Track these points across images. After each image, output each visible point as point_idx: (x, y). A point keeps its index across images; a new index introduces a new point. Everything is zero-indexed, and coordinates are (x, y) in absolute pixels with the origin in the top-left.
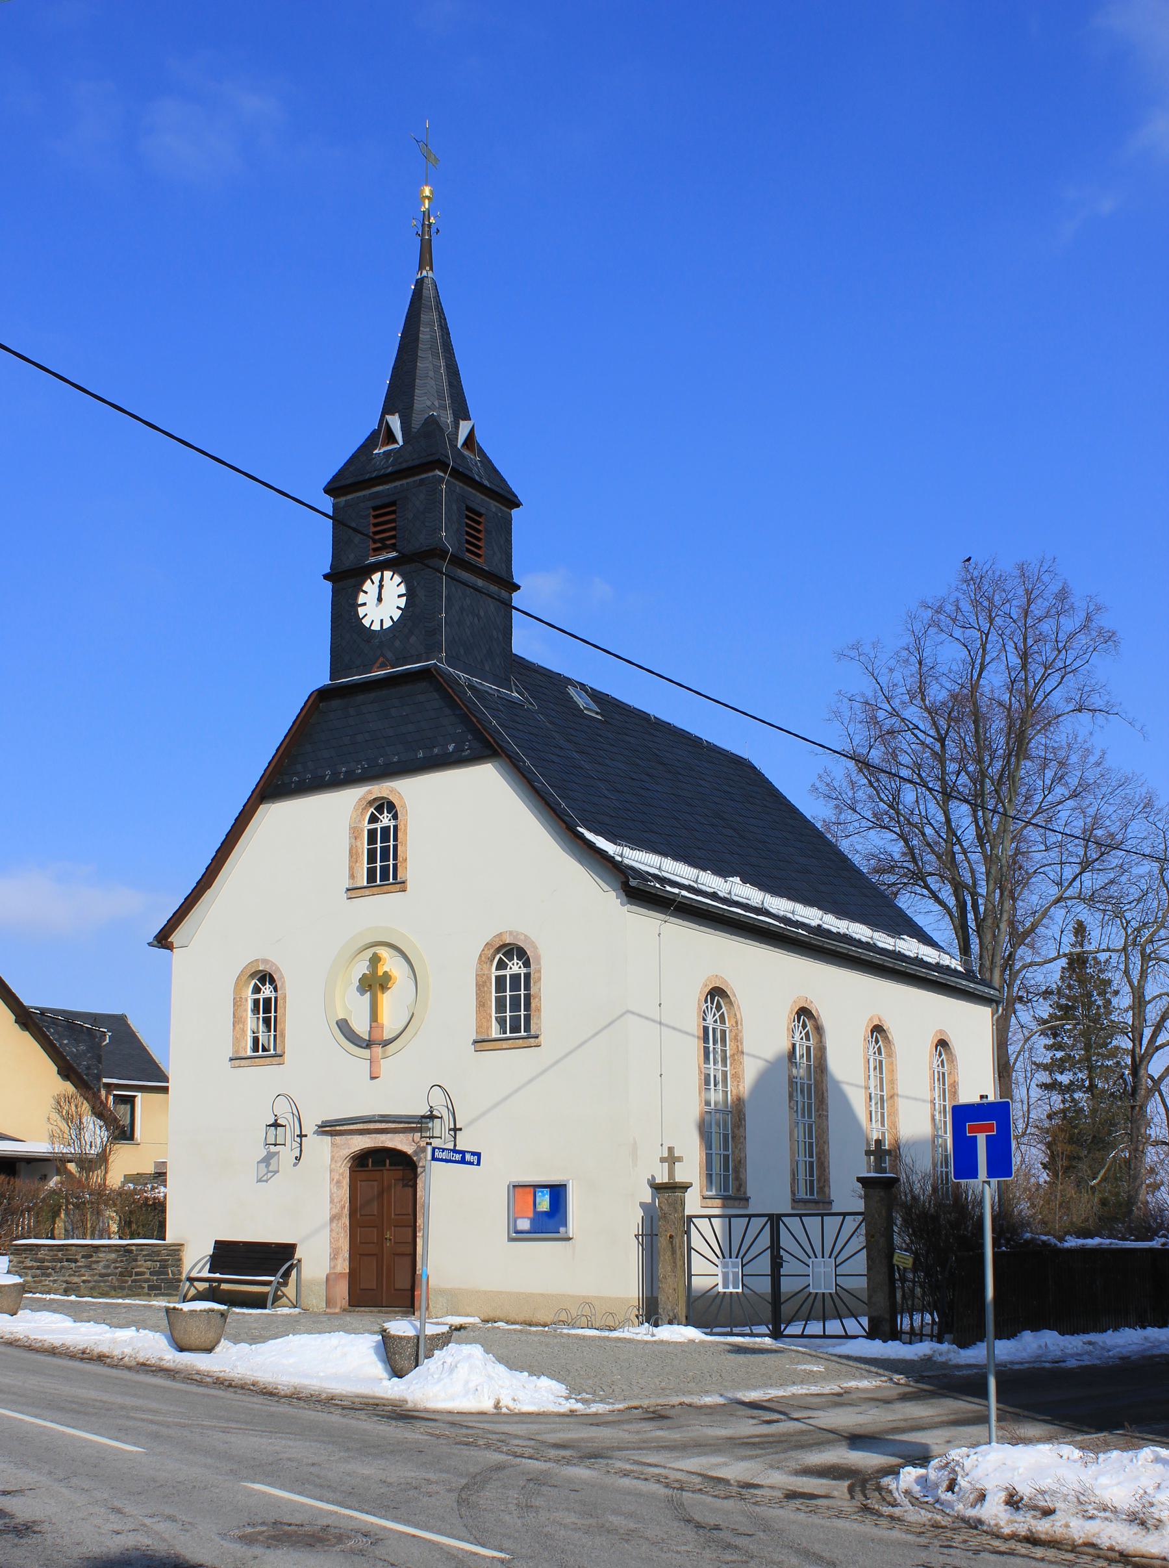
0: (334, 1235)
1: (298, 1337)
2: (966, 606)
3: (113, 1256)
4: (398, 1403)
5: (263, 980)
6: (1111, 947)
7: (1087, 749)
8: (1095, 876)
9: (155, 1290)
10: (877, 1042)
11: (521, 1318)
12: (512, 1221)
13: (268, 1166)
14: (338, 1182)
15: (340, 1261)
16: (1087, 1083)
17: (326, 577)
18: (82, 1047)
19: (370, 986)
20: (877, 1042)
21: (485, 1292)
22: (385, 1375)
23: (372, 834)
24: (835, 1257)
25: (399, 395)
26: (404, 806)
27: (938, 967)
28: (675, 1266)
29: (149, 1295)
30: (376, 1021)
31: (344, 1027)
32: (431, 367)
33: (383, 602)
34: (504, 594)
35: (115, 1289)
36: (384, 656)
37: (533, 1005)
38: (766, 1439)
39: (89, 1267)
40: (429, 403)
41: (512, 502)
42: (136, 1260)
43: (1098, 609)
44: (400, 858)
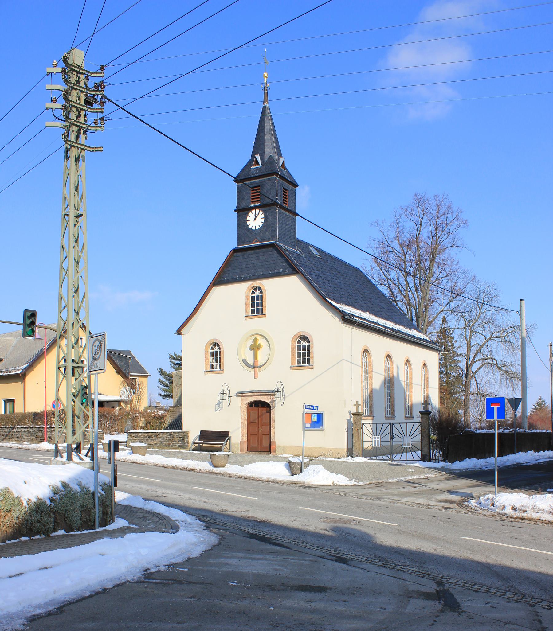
2: (415, 209)
3: (165, 436)
5: (214, 345)
9: (180, 446)
10: (366, 356)
12: (304, 424)
17: (235, 211)
18: (123, 363)
20: (366, 356)
23: (253, 298)
24: (411, 434)
25: (259, 147)
26: (265, 289)
27: (423, 340)
31: (244, 361)
35: (166, 446)
41: (296, 185)
43: (461, 211)
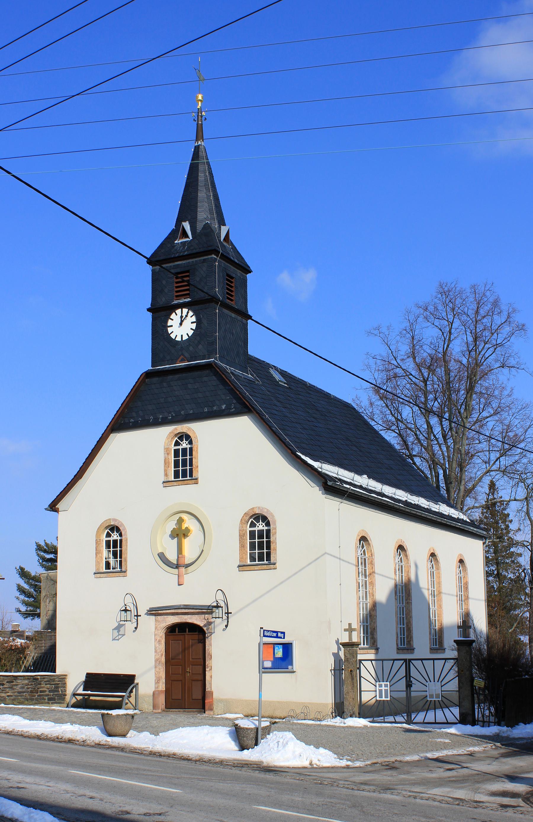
0: (157, 670)
1: (184, 729)
2: (440, 307)
3: (26, 682)
4: (258, 763)
6: (517, 498)
7: (503, 388)
8: (507, 458)
9: (52, 700)
11: (267, 715)
12: (261, 662)
13: (119, 632)
14: (159, 641)
15: (161, 684)
16: (496, 572)
17: (149, 310)
19: (178, 535)
21: (246, 701)
22: (236, 748)
23: (176, 452)
26: (196, 437)
27: (458, 520)
28: (354, 686)
29: (49, 703)
30: (181, 554)
31: (162, 557)
32: (206, 196)
33: (182, 326)
34: (244, 321)
35: (27, 700)
36: (183, 355)
37: (272, 547)
38: (458, 779)
39: (11, 688)
40: (205, 216)
41: (247, 270)
42: (40, 684)
43: (514, 311)
44: (194, 466)
